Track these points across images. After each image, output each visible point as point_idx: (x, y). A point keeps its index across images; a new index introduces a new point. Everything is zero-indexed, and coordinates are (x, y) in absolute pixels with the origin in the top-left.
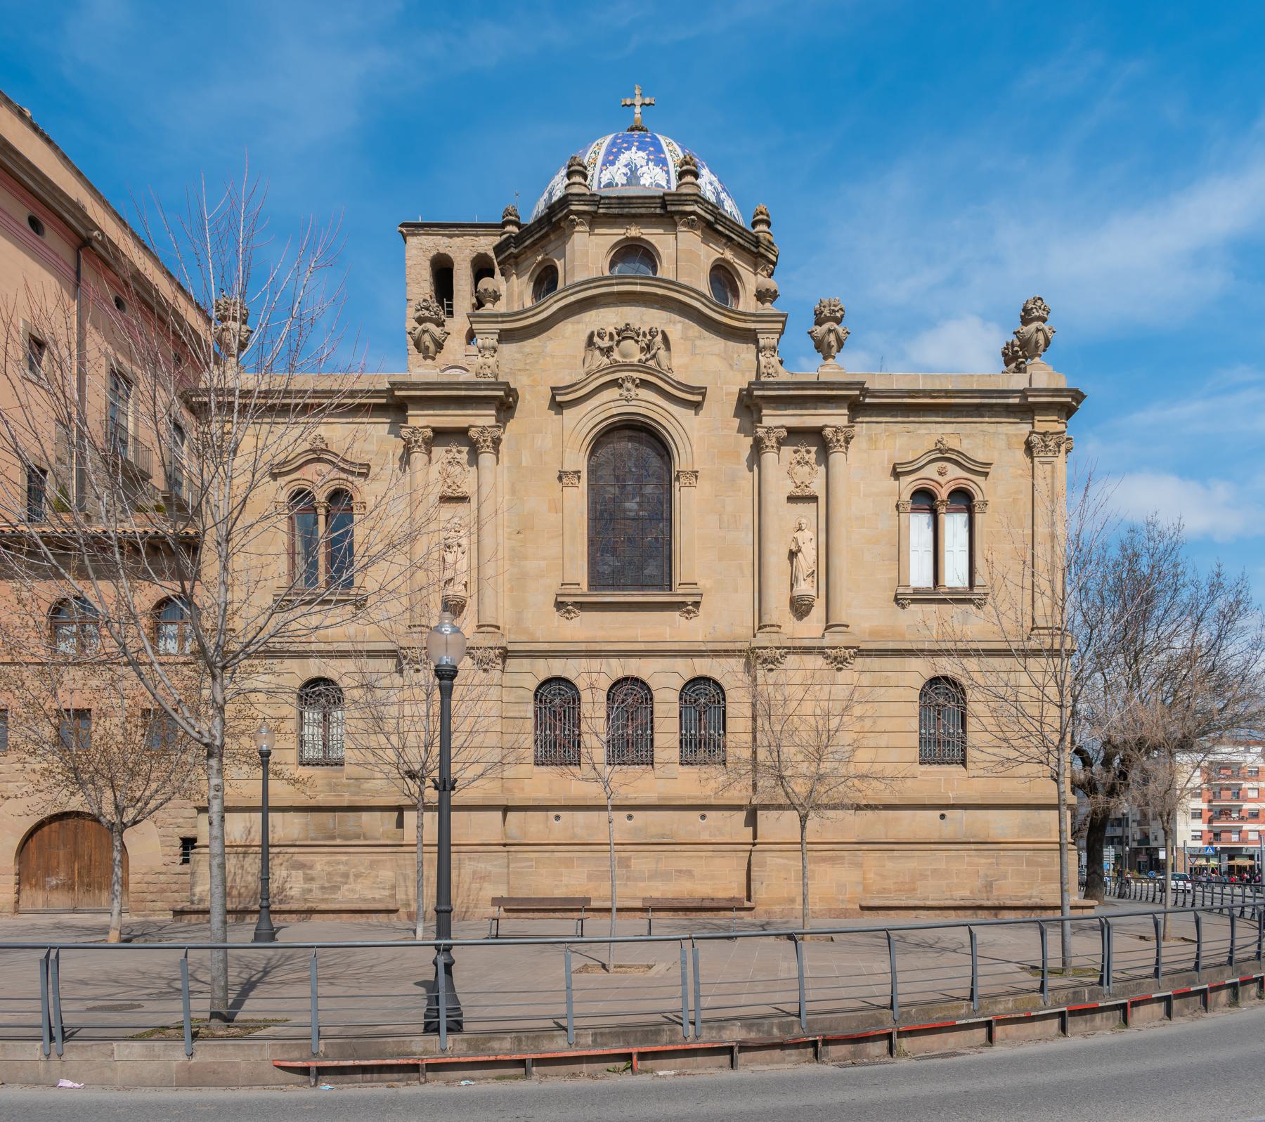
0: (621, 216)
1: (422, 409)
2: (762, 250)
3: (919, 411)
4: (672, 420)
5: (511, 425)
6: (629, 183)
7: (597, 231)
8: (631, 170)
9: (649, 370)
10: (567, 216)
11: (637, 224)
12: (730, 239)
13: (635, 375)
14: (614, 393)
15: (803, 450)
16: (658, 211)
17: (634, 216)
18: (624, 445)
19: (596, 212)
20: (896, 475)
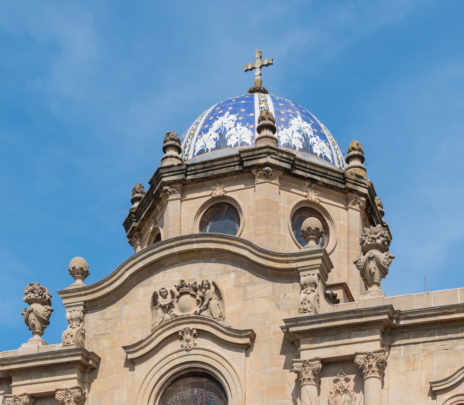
0: (207, 178)
1: (22, 380)
2: (349, 186)
3: (456, 327)
5: (96, 385)
6: (218, 147)
7: (188, 196)
8: (220, 135)
9: (204, 321)
10: (161, 187)
11: (220, 183)
12: (315, 181)
13: (191, 326)
15: (342, 379)
16: (237, 168)
17: (218, 177)
18: (187, 392)
20: (434, 394)
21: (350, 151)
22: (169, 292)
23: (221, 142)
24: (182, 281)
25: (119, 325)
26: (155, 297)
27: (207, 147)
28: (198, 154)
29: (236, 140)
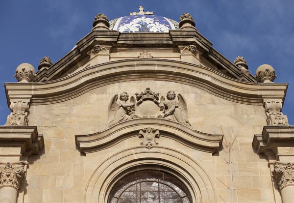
4: (192, 163)
8: (142, 25)
14: (134, 141)
19: (115, 42)
21: (237, 62)
22: (130, 98)
24: (149, 89)
25: (67, 119)
26: (115, 99)
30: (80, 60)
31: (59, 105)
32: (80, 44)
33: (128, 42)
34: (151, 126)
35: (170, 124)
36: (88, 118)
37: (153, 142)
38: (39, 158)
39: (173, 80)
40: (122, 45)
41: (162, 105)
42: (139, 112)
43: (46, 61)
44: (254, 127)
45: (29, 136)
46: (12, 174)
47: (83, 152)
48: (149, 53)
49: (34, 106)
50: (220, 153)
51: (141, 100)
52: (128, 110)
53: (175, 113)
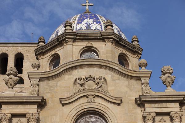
8: (88, 25)
21: (134, 39)
23: (88, 26)
24: (91, 75)
25: (56, 88)
26: (76, 80)
27: (82, 28)
28: (78, 30)
29: (95, 28)
30: (58, 44)
31: (52, 81)
32: (59, 37)
33: (81, 38)
34: (92, 93)
35: (100, 92)
36: (65, 88)
37: (92, 100)
38: (45, 108)
39: (101, 68)
40: (79, 39)
41: (96, 82)
42: (86, 86)
43: (42, 39)
44: (136, 92)
45: (40, 101)
46: (34, 118)
47: (63, 105)
48: (91, 42)
49: (41, 82)
50: (121, 104)
51: (87, 80)
52: (82, 85)
53: (102, 87)
